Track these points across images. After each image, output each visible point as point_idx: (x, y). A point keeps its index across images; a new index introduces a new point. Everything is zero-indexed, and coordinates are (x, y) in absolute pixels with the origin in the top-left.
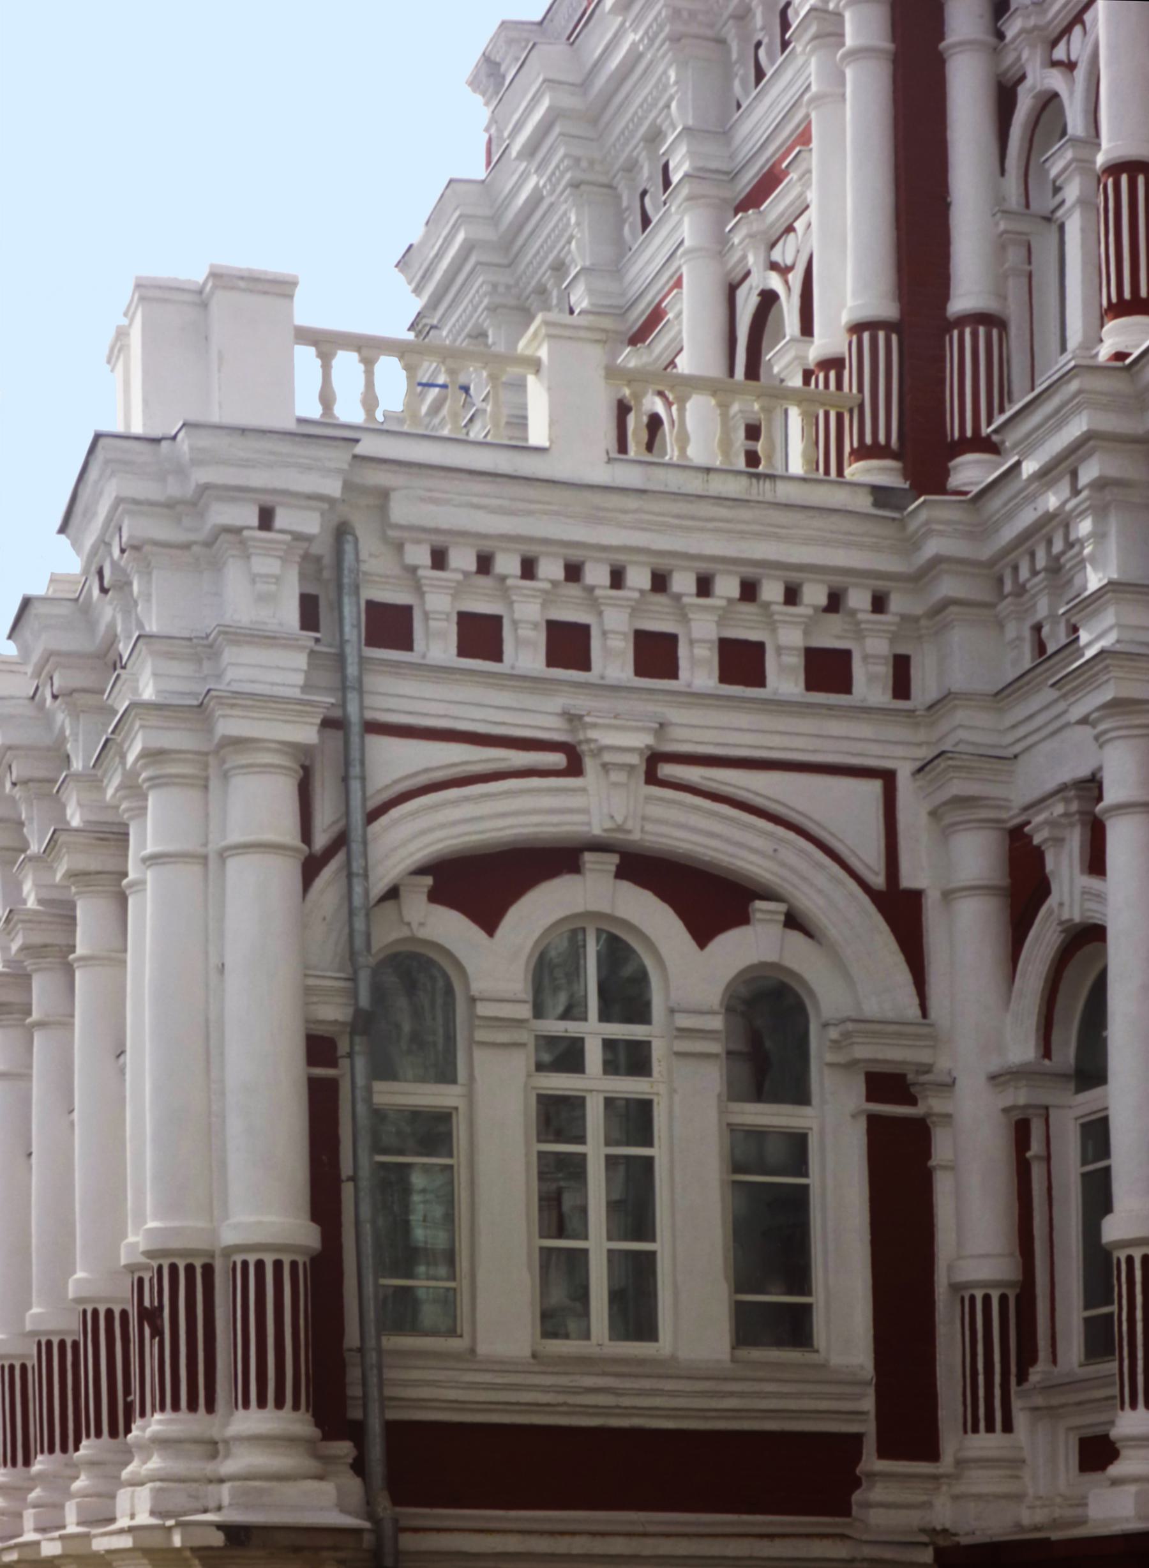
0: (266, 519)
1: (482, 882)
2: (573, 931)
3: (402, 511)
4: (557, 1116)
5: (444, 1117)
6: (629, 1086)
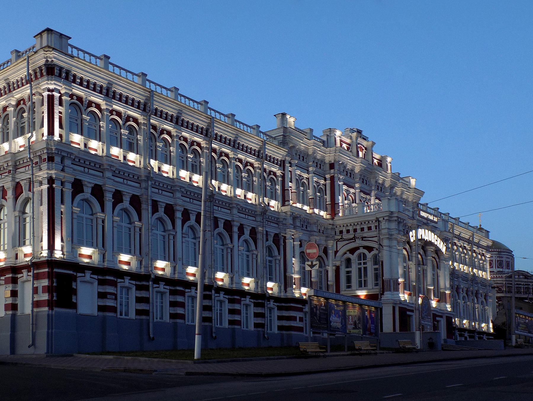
0: (384, 219)
1: (352, 251)
2: (360, 254)
4: (360, 269)
6: (365, 266)
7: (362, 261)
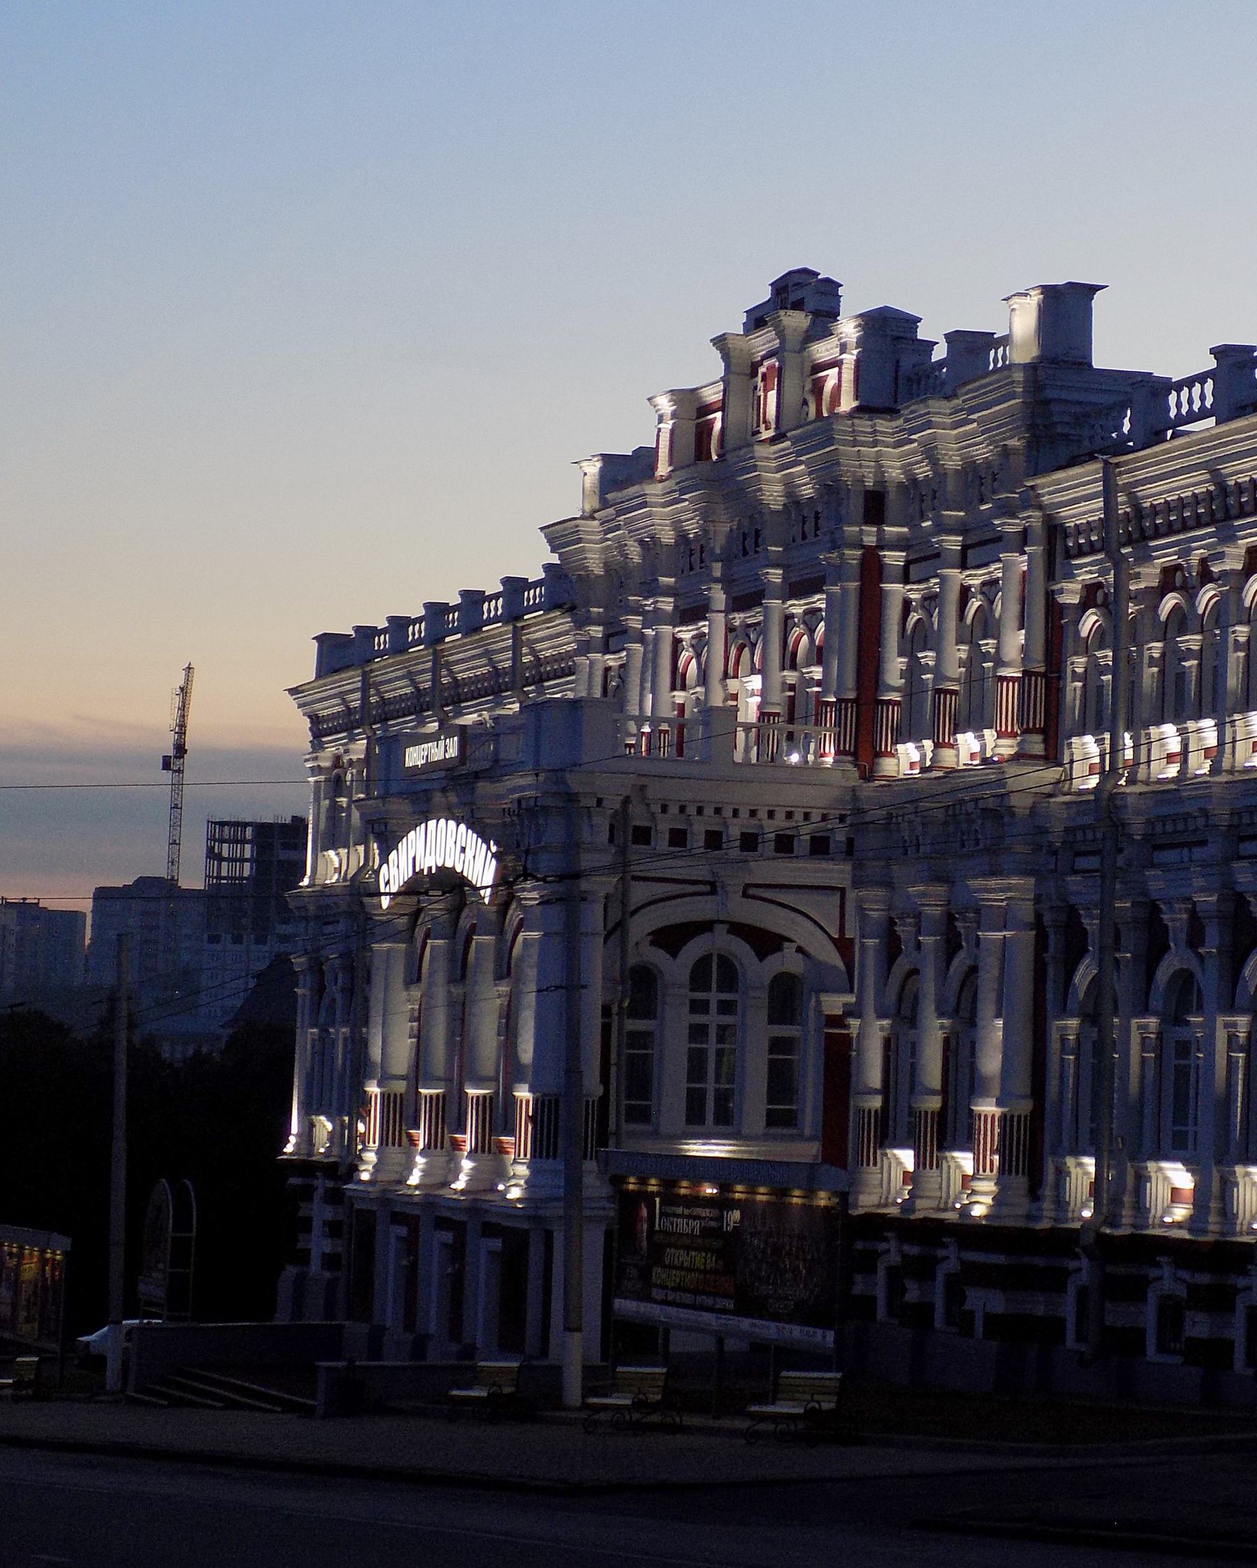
1: (671, 938)
3: (650, 794)
4: (698, 1032)
5: (648, 1034)
7: (714, 997)
